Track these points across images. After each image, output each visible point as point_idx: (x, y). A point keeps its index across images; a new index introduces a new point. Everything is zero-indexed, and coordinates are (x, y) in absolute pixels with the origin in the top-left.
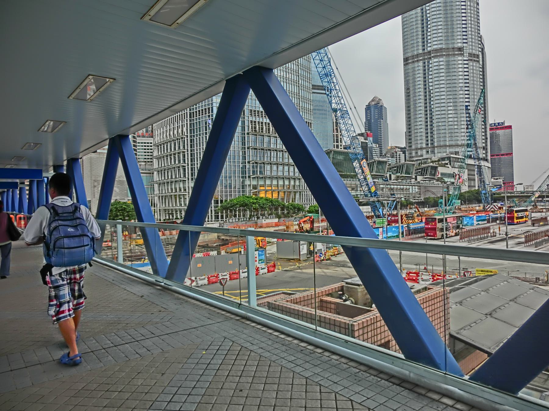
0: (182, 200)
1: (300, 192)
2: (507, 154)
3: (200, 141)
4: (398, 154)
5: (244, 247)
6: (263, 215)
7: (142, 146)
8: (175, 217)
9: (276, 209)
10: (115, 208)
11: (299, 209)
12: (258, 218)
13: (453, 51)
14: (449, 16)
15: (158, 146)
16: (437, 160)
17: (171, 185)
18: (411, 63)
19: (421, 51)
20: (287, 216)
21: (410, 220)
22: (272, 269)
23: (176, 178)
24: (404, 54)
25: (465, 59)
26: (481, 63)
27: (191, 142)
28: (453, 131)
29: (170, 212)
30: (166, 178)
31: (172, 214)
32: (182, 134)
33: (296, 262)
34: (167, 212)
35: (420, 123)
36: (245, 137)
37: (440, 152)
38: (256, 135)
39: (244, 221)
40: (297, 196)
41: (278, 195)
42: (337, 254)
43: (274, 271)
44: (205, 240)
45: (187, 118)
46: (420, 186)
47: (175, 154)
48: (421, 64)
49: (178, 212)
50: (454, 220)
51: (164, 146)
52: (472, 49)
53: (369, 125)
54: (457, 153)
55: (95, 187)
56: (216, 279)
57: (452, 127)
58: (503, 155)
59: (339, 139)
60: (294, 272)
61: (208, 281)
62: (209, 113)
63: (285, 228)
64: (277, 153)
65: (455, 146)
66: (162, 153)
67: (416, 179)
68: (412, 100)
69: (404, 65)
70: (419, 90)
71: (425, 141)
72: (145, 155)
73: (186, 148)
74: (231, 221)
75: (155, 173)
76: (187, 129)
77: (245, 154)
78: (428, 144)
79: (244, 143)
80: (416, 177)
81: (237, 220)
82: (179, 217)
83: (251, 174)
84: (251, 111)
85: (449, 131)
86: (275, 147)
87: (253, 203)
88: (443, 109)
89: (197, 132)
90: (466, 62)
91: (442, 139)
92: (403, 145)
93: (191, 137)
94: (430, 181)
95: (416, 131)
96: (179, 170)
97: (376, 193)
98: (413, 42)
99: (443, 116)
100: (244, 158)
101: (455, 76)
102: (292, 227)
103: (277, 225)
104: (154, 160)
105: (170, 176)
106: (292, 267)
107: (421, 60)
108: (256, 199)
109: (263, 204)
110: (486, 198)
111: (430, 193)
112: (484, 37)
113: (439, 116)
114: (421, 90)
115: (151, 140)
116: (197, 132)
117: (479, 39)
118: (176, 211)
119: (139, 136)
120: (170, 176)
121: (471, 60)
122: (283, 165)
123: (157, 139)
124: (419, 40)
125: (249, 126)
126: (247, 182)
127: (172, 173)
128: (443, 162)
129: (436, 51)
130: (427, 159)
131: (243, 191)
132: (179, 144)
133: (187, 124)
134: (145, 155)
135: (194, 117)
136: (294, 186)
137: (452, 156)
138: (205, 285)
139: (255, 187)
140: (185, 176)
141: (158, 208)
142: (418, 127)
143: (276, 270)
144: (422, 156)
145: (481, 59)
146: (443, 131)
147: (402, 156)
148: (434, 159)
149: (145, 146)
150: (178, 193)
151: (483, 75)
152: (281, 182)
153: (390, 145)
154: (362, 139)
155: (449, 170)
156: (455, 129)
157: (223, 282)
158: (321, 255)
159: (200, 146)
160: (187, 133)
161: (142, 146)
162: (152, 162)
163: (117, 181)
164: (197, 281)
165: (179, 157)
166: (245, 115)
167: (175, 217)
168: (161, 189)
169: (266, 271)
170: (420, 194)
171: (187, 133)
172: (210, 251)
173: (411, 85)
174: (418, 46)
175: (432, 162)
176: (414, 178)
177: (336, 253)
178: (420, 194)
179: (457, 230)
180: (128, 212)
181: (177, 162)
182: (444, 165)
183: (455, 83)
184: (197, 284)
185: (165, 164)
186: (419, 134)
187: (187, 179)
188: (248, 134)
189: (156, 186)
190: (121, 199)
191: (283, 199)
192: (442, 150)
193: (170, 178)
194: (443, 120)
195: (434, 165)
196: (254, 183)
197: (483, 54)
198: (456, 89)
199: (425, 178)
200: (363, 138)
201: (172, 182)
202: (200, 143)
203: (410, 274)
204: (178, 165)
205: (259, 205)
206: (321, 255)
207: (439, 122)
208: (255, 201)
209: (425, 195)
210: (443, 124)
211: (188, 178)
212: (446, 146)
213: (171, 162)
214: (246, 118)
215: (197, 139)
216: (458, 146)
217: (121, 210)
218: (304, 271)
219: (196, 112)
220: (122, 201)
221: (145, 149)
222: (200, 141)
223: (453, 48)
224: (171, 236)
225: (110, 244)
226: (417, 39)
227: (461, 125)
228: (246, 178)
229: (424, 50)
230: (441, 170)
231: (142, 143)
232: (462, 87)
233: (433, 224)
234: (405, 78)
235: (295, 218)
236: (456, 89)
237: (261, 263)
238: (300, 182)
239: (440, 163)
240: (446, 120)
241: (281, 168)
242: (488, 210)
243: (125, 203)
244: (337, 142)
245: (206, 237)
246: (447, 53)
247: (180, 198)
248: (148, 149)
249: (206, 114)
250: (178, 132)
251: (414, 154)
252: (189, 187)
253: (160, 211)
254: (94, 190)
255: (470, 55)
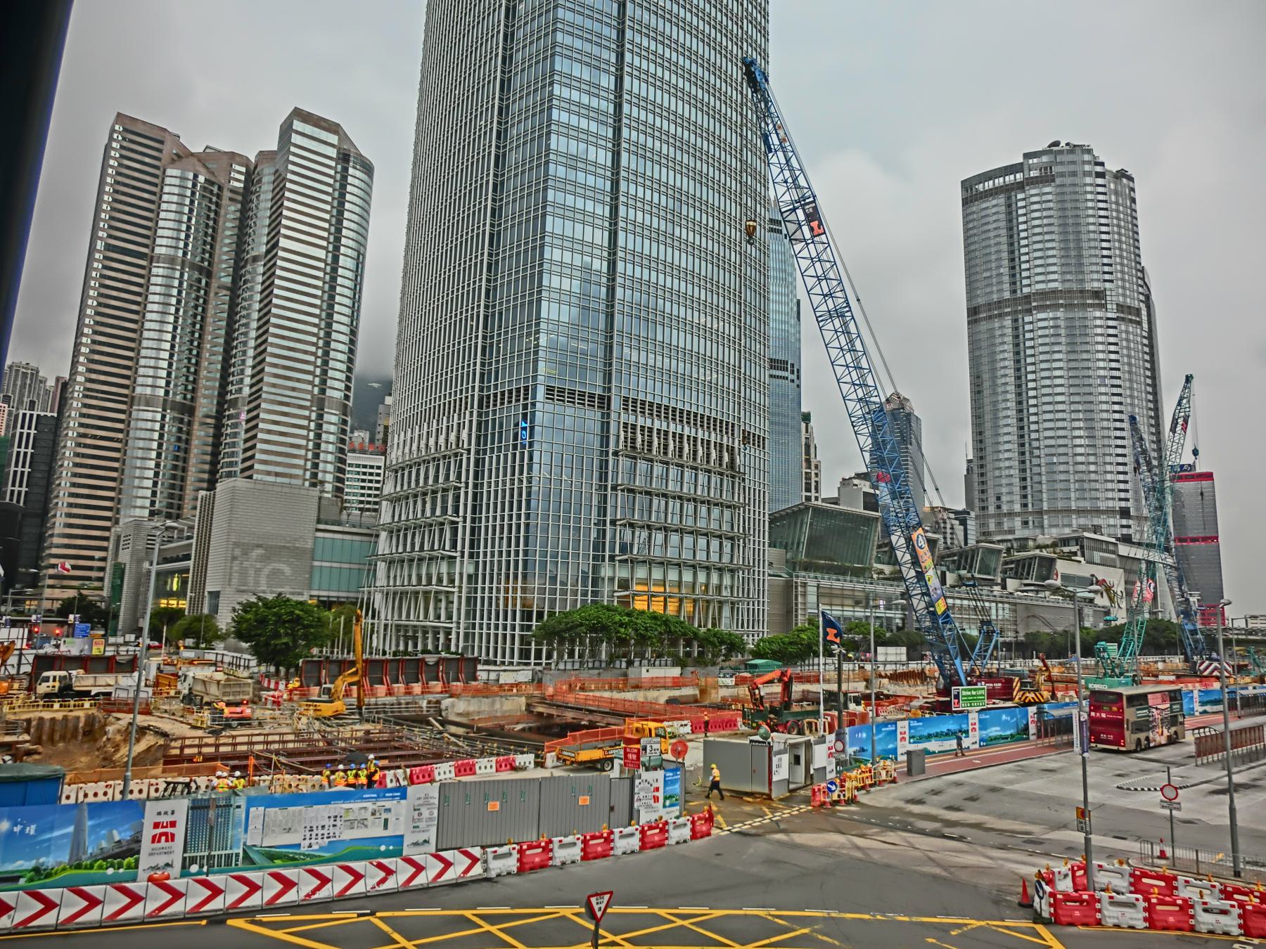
0: (443, 605)
1: (733, 603)
2: (1205, 539)
3: (498, 463)
4: (948, 526)
5: (626, 757)
6: (642, 656)
7: (358, 473)
8: (420, 647)
9: (674, 643)
10: (275, 614)
11: (734, 646)
12: (630, 663)
13: (1082, 297)
14: (1070, 221)
15: (396, 472)
16: (1049, 542)
17: (419, 566)
18: (985, 318)
19: (1007, 295)
20: (701, 661)
21: (1029, 691)
22: (704, 828)
23: (432, 549)
24: (969, 299)
25: (1110, 315)
26: (1145, 326)
27: (477, 465)
28: (1085, 477)
29: (410, 633)
30: (408, 549)
31: (415, 639)
32: (458, 445)
33: (761, 803)
34: (402, 633)
35: (1007, 455)
36: (607, 461)
37: (1057, 526)
38: (635, 458)
39: (593, 668)
40: (726, 611)
41: (680, 606)
42: (871, 786)
43: (709, 834)
44: (494, 714)
45: (472, 407)
46: (1015, 604)
47: (434, 492)
48: (1008, 322)
49: (430, 635)
50: (1164, 701)
51: (410, 473)
52: (1124, 295)
53: (878, 457)
54: (1096, 529)
55: (234, 558)
56: (544, 857)
57: (1082, 468)
58: (1194, 540)
59: (813, 484)
60: (769, 841)
61: (519, 860)
62: (526, 399)
63: (697, 692)
64: (682, 505)
65: (1090, 511)
66: (405, 487)
67: (1004, 587)
68: (987, 401)
69: (969, 323)
70: (1003, 380)
71: (1018, 497)
72: (363, 495)
73: (463, 479)
74: (561, 666)
75: (384, 535)
76: (470, 436)
77: (605, 502)
78: (1025, 505)
79: (603, 476)
80: (1004, 580)
81: (577, 666)
82: (430, 647)
83: (617, 552)
84: (626, 400)
85: (1077, 477)
86: (678, 489)
87: (621, 625)
88: (1060, 424)
89: (493, 443)
90: (1111, 323)
91: (1060, 495)
92: (961, 506)
93: (477, 452)
94: (1037, 592)
95: (997, 473)
96: (441, 531)
97: (948, 616)
98: (988, 274)
99: (1061, 442)
100: (602, 511)
101: (1088, 352)
102: (713, 691)
103: (677, 684)
104: (384, 503)
105: (420, 543)
106: (757, 822)
107: (1008, 314)
108: (629, 615)
109: (646, 629)
110: (1196, 641)
111: (1039, 623)
112: (1148, 270)
113: (1052, 442)
114: (1008, 380)
115: (379, 460)
116: (493, 443)
117: (1140, 274)
118: (425, 633)
119: (353, 451)
120: (420, 543)
121: (1123, 319)
122: (695, 533)
123: (395, 455)
124: (1002, 270)
125: (618, 437)
126: (606, 571)
127: (423, 538)
128: (1066, 549)
129: (1043, 294)
130: (1026, 539)
131: (595, 594)
132: (448, 469)
133: (471, 422)
134: (363, 495)
135: (488, 407)
136: (719, 588)
137: (1086, 534)
138: (509, 874)
139: (624, 584)
140: (454, 546)
141: (383, 622)
142: (1002, 464)
143: (714, 831)
144: (1011, 531)
145: (1145, 318)
146: (1062, 477)
147: (959, 529)
148: (1042, 539)
149: (364, 474)
150: (434, 588)
151: (1152, 354)
152: (687, 577)
153: (927, 504)
154: (866, 487)
155: (1081, 569)
156: (1090, 472)
157: (596, 907)
158: (833, 788)
159: (497, 476)
160: (470, 444)
161: (358, 473)
162: (375, 510)
163: (199, 438)
164: (486, 862)
165: (444, 501)
166: (612, 407)
167: (420, 647)
168: (392, 575)
169: (686, 832)
170: (1015, 623)
171: (470, 444)
172: (516, 752)
173: (985, 368)
174: (1000, 283)
175: (1039, 547)
176: (997, 584)
177: (868, 782)
178: (1015, 623)
179: (1173, 729)
180: (305, 627)
181: (438, 512)
182: (1069, 557)
183: (1089, 368)
184: (485, 870)
185: (409, 513)
186: (1004, 481)
187: (458, 554)
188: (616, 454)
189: (382, 566)
190: (293, 594)
191: (691, 618)
192: (1061, 520)
193: (417, 548)
194: (1061, 450)
195: (1045, 553)
196: (623, 573)
197: (1148, 307)
198: (1091, 381)
199: (1026, 585)
200: (868, 484)
201: (421, 560)
202: (498, 469)
203: (1145, 880)
204: (440, 519)
205: (636, 630)
206: (833, 788)
207: (1053, 455)
208: (627, 619)
209: (1027, 625)
210: (1063, 459)
211: (463, 553)
212: (1068, 511)
213: (423, 511)
214: (613, 416)
215: (491, 458)
216: (1097, 512)
217: (288, 621)
218: (798, 838)
219: (495, 395)
220: (295, 598)
221: (364, 481)
222: (498, 463)
223: (1081, 292)
224: (409, 699)
225: (248, 711)
226: (999, 267)
227: (1105, 463)
228: (603, 560)
229: (1014, 292)
230: (1062, 567)
231: (358, 466)
232: (1105, 377)
233: (1115, 709)
234: (971, 351)
235: (722, 668)
236: (1091, 381)
237: (671, 805)
238: (733, 577)
239: (1058, 550)
240: (1070, 451)
241: (674, 538)
242: (1206, 673)
243: (301, 603)
244: (808, 490)
245: (497, 706)
246: (1069, 302)
247: (438, 601)
248: (371, 481)
249: (518, 400)
250: (447, 440)
251: (992, 527)
252: (461, 574)
253: (385, 629)
254: (231, 568)
255: (1121, 308)
